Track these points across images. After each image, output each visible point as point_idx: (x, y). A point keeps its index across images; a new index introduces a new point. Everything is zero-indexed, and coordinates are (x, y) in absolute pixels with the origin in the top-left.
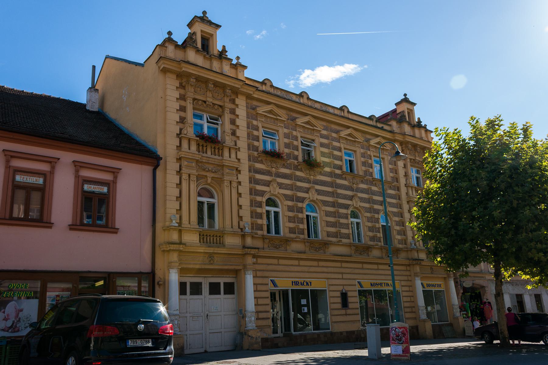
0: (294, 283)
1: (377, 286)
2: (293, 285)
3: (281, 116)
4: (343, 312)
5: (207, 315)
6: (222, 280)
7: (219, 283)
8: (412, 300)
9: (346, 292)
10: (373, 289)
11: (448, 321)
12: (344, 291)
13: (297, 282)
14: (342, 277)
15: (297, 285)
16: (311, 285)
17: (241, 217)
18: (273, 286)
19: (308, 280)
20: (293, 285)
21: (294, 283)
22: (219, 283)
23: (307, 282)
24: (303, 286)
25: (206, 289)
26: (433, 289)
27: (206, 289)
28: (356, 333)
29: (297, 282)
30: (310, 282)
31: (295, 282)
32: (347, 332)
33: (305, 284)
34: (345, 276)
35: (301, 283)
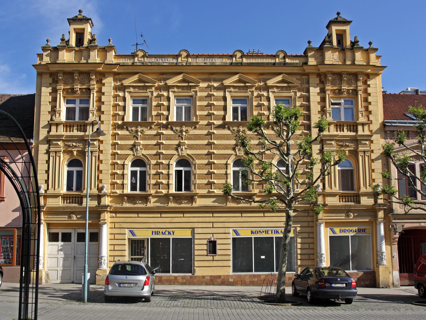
0: (154, 233)
1: (260, 233)
2: (153, 234)
3: (150, 82)
4: (211, 258)
5: (75, 257)
6: (60, 231)
7: (252, 238)
8: (310, 247)
9: (215, 240)
10: (253, 236)
11: (371, 270)
12: (212, 239)
13: (157, 232)
14: (213, 224)
15: (157, 234)
16: (173, 234)
17: (101, 180)
18: (132, 235)
19: (170, 230)
20: (153, 234)
21: (154, 233)
22: (252, 238)
23: (169, 232)
24: (165, 235)
25: (74, 237)
26: (274, 236)
27: (74, 237)
28: (222, 277)
29: (157, 232)
30: (173, 232)
31: (155, 232)
32: (211, 276)
33: (167, 233)
34: (215, 225)
35: (162, 232)
